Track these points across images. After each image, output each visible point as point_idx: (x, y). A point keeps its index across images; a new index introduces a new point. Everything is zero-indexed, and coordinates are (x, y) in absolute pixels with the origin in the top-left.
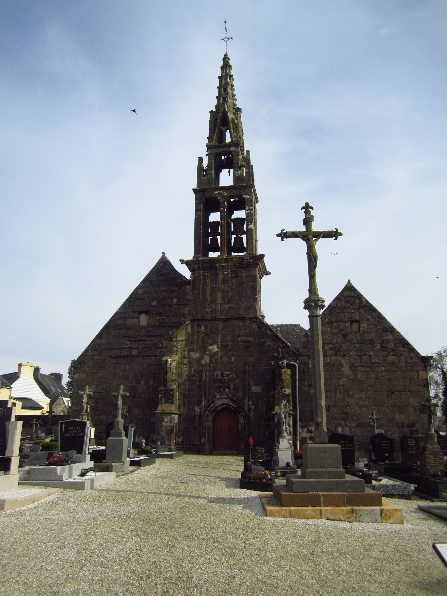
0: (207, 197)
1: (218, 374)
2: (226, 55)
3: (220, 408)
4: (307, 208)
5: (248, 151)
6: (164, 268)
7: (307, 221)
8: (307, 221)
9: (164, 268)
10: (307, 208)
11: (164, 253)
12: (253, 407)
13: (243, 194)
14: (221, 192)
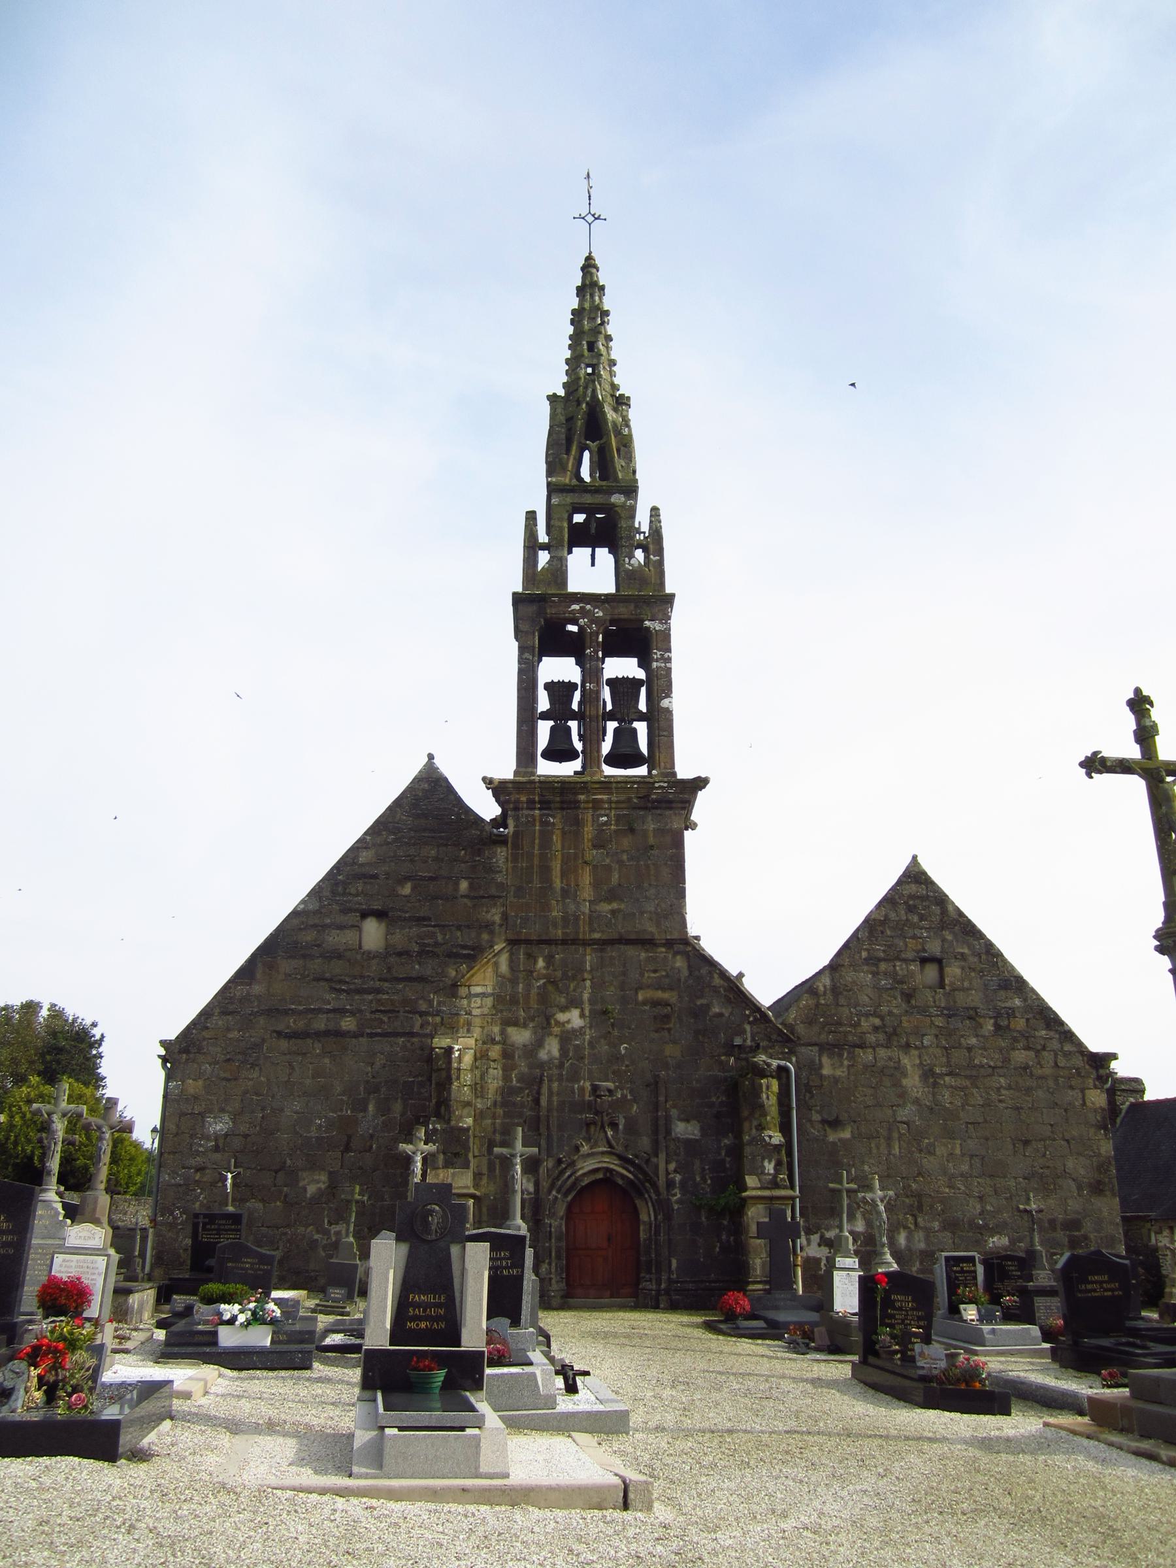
0: (544, 620)
1: (582, 1089)
2: (589, 258)
3: (586, 1181)
4: (1139, 704)
5: (655, 512)
6: (429, 797)
7: (1145, 735)
8: (1145, 735)
9: (429, 797)
10: (1139, 704)
11: (431, 757)
12: (678, 1178)
13: (636, 622)
14: (588, 607)
